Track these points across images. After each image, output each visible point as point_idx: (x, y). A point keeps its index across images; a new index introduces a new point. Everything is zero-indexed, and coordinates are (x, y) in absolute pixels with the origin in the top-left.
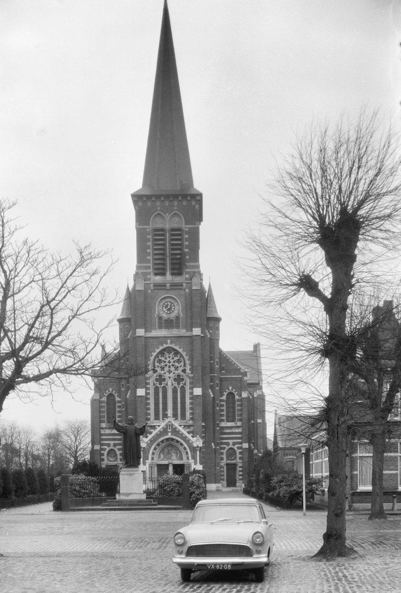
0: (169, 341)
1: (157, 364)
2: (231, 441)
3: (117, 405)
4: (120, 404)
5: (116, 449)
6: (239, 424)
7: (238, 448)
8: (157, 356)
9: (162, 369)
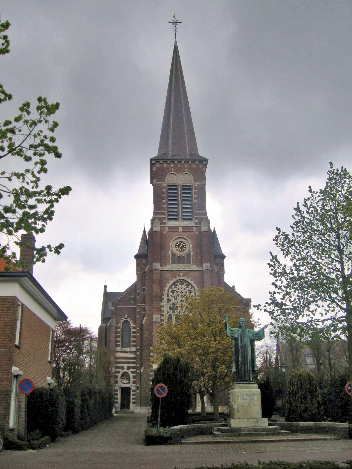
0: (181, 274)
1: (170, 294)
2: (125, 366)
3: (132, 330)
4: (134, 330)
5: (129, 372)
6: (133, 349)
7: (132, 372)
8: (171, 286)
9: (175, 298)
